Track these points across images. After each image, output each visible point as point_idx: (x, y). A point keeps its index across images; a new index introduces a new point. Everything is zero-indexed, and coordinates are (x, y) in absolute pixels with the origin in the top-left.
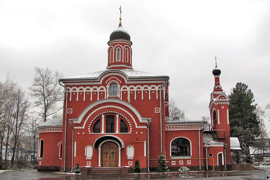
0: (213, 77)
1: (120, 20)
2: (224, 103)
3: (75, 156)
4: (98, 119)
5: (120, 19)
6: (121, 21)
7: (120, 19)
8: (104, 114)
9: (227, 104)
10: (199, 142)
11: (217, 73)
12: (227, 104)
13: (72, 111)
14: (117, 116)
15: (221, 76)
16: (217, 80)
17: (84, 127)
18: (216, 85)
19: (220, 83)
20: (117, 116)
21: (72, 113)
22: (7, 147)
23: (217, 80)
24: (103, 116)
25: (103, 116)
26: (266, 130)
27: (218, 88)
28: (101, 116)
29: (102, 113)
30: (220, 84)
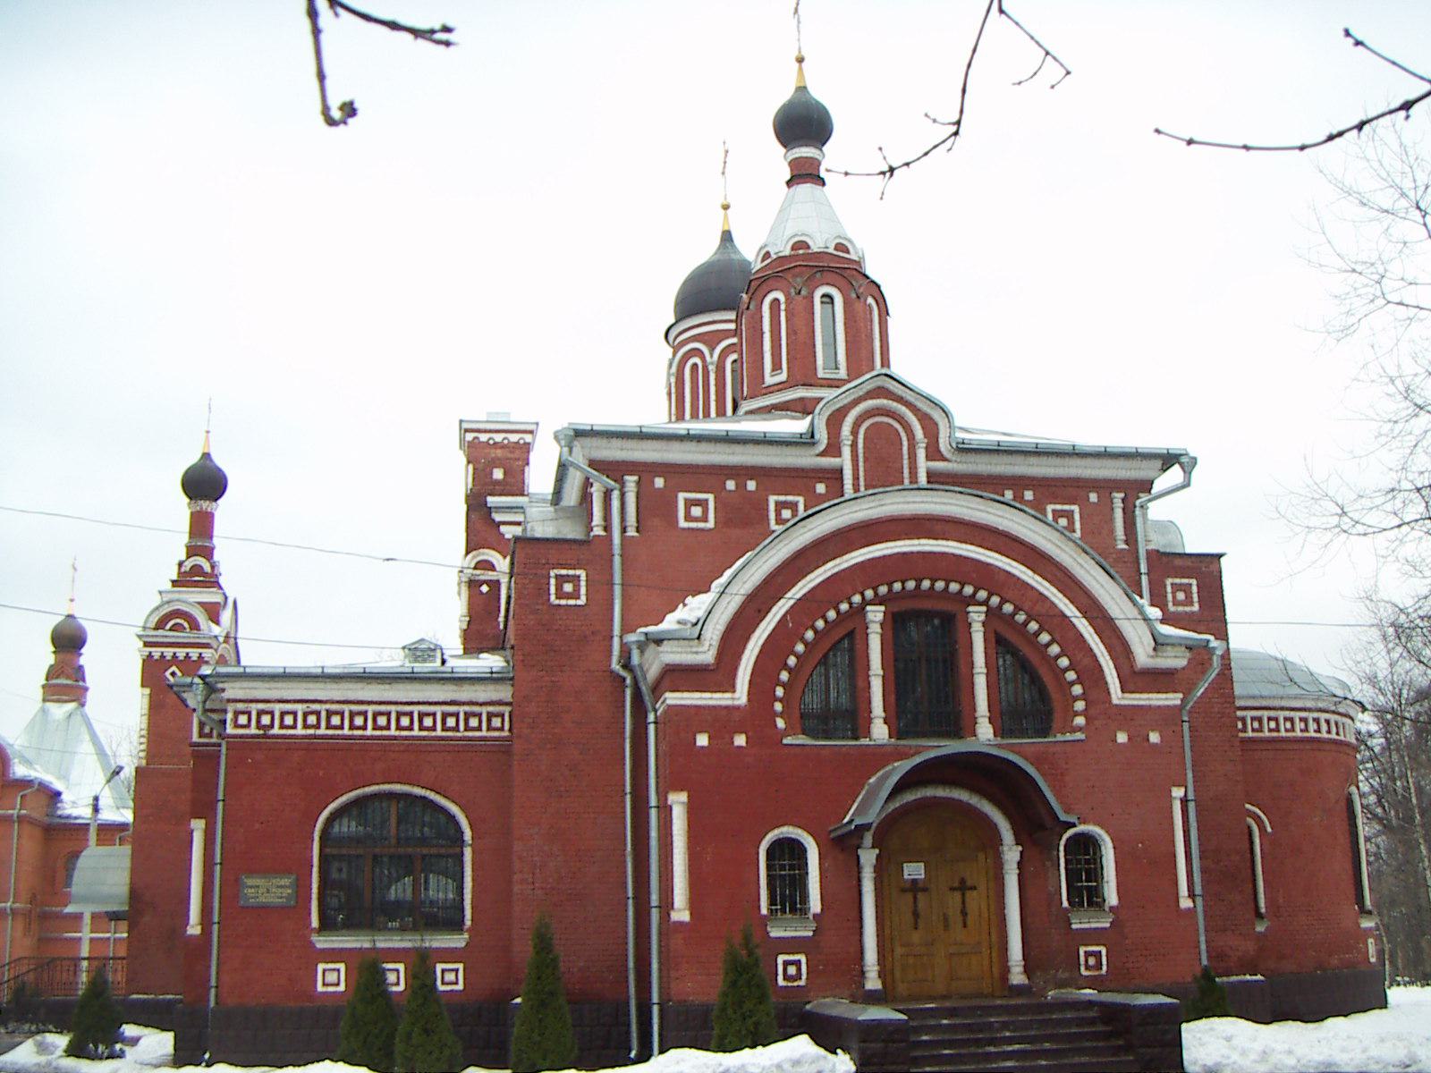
0: (180, 509)
1: (797, 65)
2: (181, 653)
3: (681, 914)
4: (841, 632)
5: (800, 60)
6: (800, 69)
7: (800, 60)
8: (879, 600)
9: (163, 656)
10: (624, 802)
11: (204, 484)
12: (163, 656)
13: (583, 590)
14: (977, 615)
15: (224, 511)
16: (202, 527)
17: (741, 696)
18: (192, 551)
19: (215, 541)
20: (977, 615)
21: (582, 601)
22: (111, 959)
23: (202, 527)
24: (876, 614)
25: (876, 614)
26: (1372, 680)
27: (197, 570)
28: (860, 611)
29: (869, 593)
30: (213, 549)
